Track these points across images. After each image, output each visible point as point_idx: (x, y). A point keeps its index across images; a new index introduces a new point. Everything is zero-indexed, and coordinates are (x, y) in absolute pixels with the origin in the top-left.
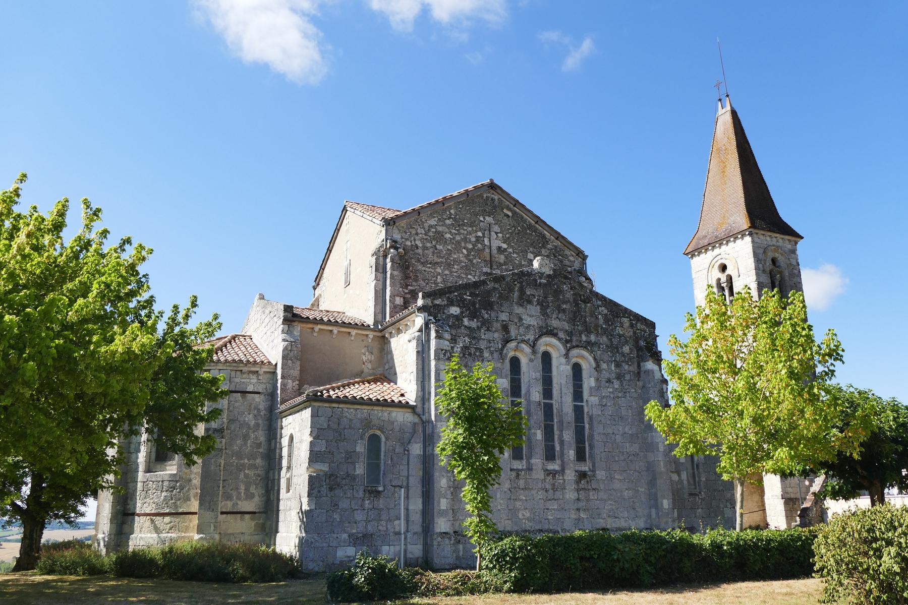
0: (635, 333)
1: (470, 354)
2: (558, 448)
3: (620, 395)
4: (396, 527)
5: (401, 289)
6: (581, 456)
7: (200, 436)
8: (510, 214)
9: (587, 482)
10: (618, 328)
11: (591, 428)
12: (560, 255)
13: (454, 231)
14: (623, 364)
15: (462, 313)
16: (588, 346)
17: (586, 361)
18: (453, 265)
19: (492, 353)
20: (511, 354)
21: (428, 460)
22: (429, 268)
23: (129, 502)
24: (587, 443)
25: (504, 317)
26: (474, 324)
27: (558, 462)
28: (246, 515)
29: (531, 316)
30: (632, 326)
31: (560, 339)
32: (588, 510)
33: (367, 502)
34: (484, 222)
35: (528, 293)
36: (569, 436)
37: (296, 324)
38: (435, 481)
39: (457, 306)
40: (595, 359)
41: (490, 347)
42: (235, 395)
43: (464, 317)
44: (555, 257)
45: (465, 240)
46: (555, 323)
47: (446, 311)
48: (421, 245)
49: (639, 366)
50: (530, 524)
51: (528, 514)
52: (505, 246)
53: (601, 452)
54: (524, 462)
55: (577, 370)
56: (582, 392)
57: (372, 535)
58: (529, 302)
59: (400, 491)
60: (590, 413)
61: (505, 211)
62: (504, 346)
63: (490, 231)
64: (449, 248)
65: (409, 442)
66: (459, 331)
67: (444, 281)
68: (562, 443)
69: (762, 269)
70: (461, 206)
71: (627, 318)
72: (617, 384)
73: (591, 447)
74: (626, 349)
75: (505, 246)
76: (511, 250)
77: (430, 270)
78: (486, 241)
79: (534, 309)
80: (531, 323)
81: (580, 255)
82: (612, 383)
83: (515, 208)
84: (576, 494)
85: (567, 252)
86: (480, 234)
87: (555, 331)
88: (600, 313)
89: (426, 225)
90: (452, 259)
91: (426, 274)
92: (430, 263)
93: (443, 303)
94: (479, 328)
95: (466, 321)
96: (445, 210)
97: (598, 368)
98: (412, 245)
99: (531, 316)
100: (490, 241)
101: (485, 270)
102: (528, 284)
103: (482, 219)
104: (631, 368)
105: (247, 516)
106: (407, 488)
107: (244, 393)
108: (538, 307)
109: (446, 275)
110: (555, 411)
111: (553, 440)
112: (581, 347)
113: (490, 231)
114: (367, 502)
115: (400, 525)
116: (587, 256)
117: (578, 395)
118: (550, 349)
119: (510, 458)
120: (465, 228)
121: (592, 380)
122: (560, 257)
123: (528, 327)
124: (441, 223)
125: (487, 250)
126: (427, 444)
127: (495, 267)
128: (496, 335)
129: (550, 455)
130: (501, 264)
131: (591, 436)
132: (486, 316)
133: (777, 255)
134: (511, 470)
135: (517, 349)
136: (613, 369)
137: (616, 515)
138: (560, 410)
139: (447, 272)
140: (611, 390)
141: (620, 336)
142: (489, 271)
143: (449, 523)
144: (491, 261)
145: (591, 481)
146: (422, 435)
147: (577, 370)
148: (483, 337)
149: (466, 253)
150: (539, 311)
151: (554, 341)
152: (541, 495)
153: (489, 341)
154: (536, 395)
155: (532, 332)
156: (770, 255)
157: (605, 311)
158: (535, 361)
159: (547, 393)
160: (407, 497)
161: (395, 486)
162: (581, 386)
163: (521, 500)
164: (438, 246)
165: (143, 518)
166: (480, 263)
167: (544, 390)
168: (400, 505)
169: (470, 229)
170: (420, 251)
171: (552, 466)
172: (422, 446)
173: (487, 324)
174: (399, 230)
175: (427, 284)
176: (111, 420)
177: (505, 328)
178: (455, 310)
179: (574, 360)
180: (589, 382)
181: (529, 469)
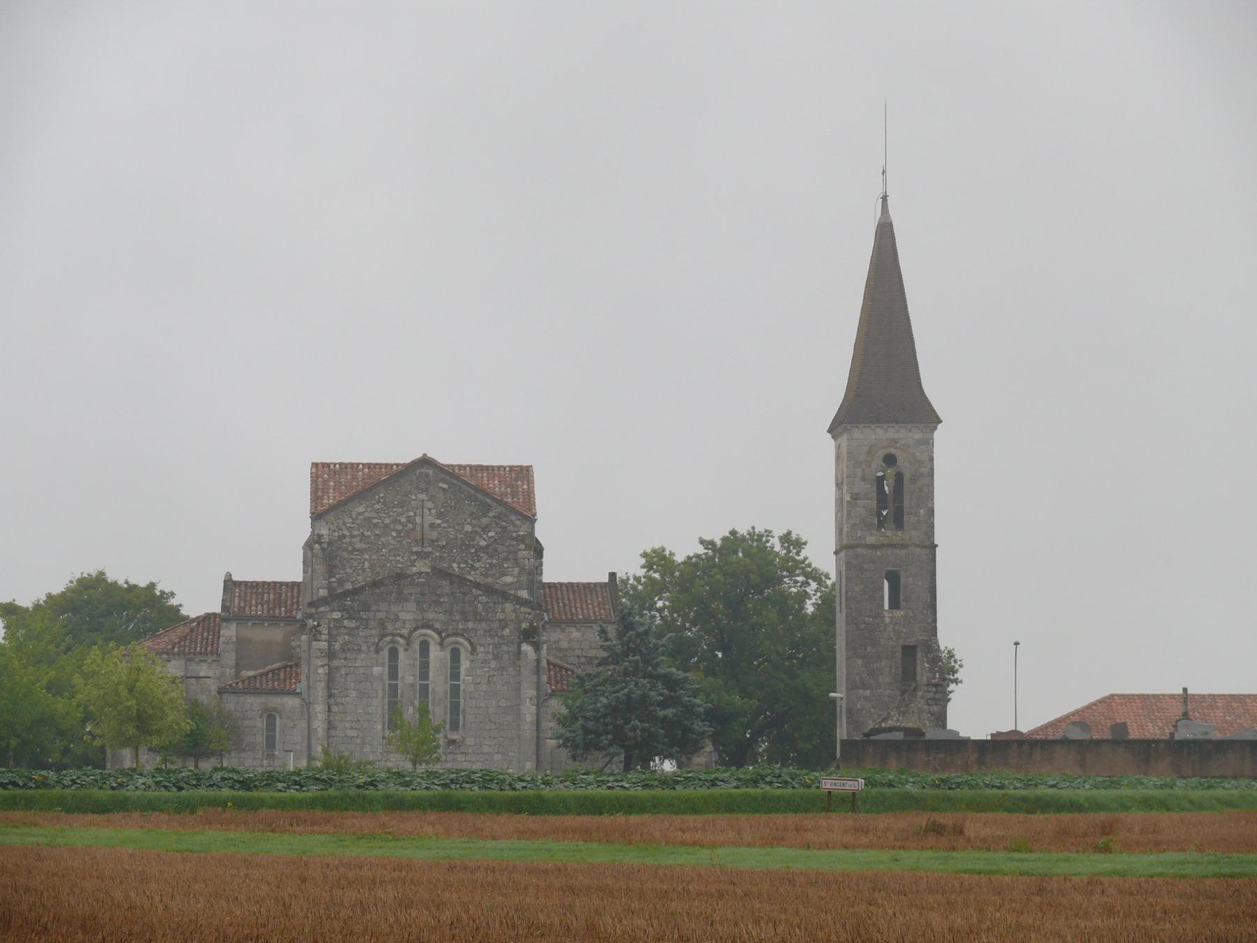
7: (817, 586)
8: (445, 486)
13: (383, 515)
18: (381, 549)
21: (310, 732)
25: (381, 615)
26: (353, 624)
31: (434, 630)
33: (265, 762)
34: (416, 500)
40: (471, 643)
42: (191, 679)
45: (396, 521)
46: (430, 615)
48: (348, 534)
52: (438, 522)
56: (428, 672)
58: (406, 600)
61: (440, 485)
67: (371, 567)
72: (493, 664)
75: (438, 522)
76: (445, 525)
77: (358, 557)
78: (418, 520)
79: (412, 606)
85: (513, 517)
87: (431, 623)
90: (380, 543)
92: (357, 551)
95: (346, 622)
98: (339, 536)
99: (408, 614)
101: (415, 549)
103: (413, 497)
107: (198, 678)
108: (415, 604)
110: (430, 690)
113: (423, 508)
122: (504, 523)
123: (404, 622)
125: (418, 529)
127: (426, 544)
128: (373, 632)
130: (433, 541)
135: (392, 641)
141: (500, 621)
148: (361, 634)
151: (429, 632)
153: (366, 637)
156: (881, 453)
159: (424, 675)
164: (366, 533)
169: (401, 510)
170: (347, 540)
173: (365, 623)
176: (64, 787)
177: (382, 624)
178: (337, 615)
180: (465, 664)
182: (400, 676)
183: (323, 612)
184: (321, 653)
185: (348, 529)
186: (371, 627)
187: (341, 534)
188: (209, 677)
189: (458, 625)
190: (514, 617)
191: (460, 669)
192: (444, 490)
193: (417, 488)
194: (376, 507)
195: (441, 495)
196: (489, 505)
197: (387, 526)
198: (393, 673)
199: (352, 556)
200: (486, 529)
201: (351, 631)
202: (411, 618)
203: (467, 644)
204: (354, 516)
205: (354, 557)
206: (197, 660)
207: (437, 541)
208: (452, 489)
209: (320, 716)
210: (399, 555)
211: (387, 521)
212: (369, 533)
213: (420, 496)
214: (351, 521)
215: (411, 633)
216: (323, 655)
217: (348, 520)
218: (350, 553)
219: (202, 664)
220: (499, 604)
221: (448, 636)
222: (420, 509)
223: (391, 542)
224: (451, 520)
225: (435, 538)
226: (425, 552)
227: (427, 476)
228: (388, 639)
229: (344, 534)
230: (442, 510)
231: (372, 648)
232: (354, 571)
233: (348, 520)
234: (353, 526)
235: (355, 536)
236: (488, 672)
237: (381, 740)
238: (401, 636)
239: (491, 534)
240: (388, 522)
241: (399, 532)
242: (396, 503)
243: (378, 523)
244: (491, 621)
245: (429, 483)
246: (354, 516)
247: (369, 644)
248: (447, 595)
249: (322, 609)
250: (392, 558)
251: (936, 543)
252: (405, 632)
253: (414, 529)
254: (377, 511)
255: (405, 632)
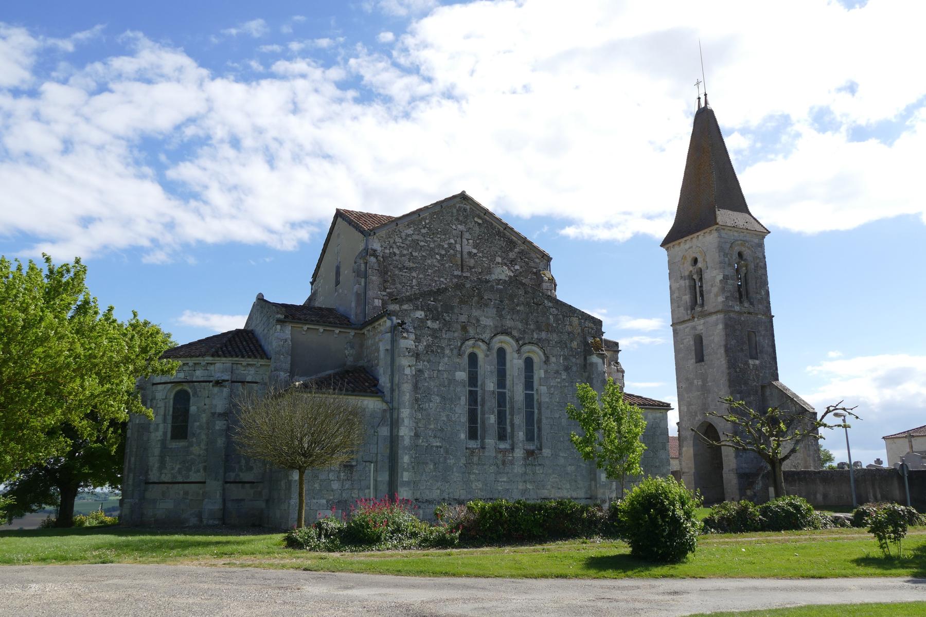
0: (583, 330)
1: (432, 351)
2: (509, 430)
3: (567, 384)
4: (367, 495)
5: (379, 292)
6: (530, 437)
8: (480, 221)
9: (534, 458)
10: (567, 326)
11: (540, 413)
12: (526, 258)
13: (429, 239)
14: (571, 358)
15: (426, 316)
16: (538, 343)
17: (537, 355)
18: (427, 270)
19: (452, 350)
20: (469, 351)
21: (394, 440)
22: (406, 272)
23: (150, 472)
24: (535, 426)
25: (463, 318)
26: (436, 325)
27: (509, 441)
28: (246, 485)
29: (488, 319)
30: (580, 324)
31: (513, 337)
32: (534, 482)
33: (342, 474)
35: (486, 297)
36: (519, 420)
37: (287, 324)
38: (399, 457)
39: (422, 310)
40: (545, 354)
41: (450, 345)
42: (236, 384)
43: (427, 320)
44: (522, 259)
46: (509, 323)
47: (412, 315)
49: (585, 359)
50: (482, 494)
51: (480, 486)
52: (475, 251)
53: (548, 434)
54: (479, 442)
55: (529, 363)
57: (346, 501)
58: (486, 305)
59: (370, 465)
60: (539, 400)
61: (476, 219)
62: (462, 344)
63: (461, 238)
64: (424, 254)
65: (379, 425)
66: (423, 331)
67: (419, 284)
68: (512, 425)
69: (727, 262)
70: (435, 216)
71: (576, 317)
73: (540, 429)
74: (575, 344)
75: (475, 251)
76: (481, 255)
78: (458, 247)
79: (492, 311)
80: (487, 324)
81: (545, 257)
82: (561, 374)
83: (485, 217)
84: (524, 469)
86: (452, 241)
87: (509, 330)
88: (551, 314)
89: (403, 235)
91: (403, 277)
92: (407, 269)
93: (410, 308)
94: (440, 330)
95: (429, 323)
96: (421, 221)
97: (547, 361)
99: (488, 319)
100: (461, 246)
101: (456, 273)
102: (485, 291)
104: (578, 361)
105: (248, 486)
106: (376, 462)
107: (243, 382)
109: (421, 278)
110: (508, 398)
111: (505, 424)
112: (533, 343)
113: (461, 238)
114: (342, 474)
115: (370, 493)
116: (551, 259)
117: (529, 385)
118: (504, 345)
119: (466, 438)
120: (439, 236)
121: (542, 372)
122: (527, 260)
124: (416, 233)
125: (459, 255)
126: (394, 427)
129: (502, 436)
130: (471, 268)
131: (540, 421)
132: (447, 318)
133: (743, 249)
134: (466, 448)
135: (474, 346)
136: (562, 362)
137: (559, 487)
138: (512, 398)
139: (421, 276)
140: (559, 380)
142: (459, 273)
143: (411, 492)
144: (462, 265)
145: (537, 458)
146: (389, 420)
147: (529, 363)
148: (444, 336)
149: (439, 258)
150: (495, 313)
151: (508, 339)
152: (493, 469)
153: (449, 340)
154: (491, 385)
155: (488, 331)
156: (737, 249)
157: (556, 312)
158: (490, 357)
159: (501, 383)
160: (376, 471)
161: (366, 462)
162: (532, 377)
163: (474, 473)
164: (414, 254)
165: (907, 444)
166: (452, 267)
167: (498, 380)
168: (370, 476)
169: (444, 237)
170: (397, 257)
171: (502, 446)
172: (389, 429)
173: (447, 325)
174: (379, 240)
175: (403, 286)
177: (464, 328)
179: (526, 355)
180: (539, 373)
181: (483, 448)
182: (479, 383)
183: (406, 310)
184: (409, 353)
185: (398, 247)
186: (454, 330)
187: (391, 251)
188: (256, 383)
189: (533, 334)
190: (580, 330)
191: (533, 379)
192: (479, 224)
193: (457, 219)
194: (423, 231)
195: (477, 228)
196: (514, 242)
197: (432, 249)
198: (473, 379)
199: (401, 273)
200: (513, 262)
201: (434, 334)
202: (491, 324)
203: (541, 353)
204: (404, 237)
205: (404, 274)
206: (244, 363)
207: (474, 267)
208: (486, 225)
209: (406, 422)
210: (443, 277)
211: (432, 245)
212: (417, 254)
213: (459, 227)
214: (401, 241)
215: (492, 338)
216: (411, 354)
217: (398, 240)
218: (400, 269)
219: (250, 368)
220: (567, 317)
221: (525, 344)
222: (459, 238)
223: (435, 264)
224: (485, 251)
225: (472, 265)
226: (464, 277)
227: (465, 210)
228: (471, 342)
229: (394, 252)
230: (478, 242)
231: (455, 352)
232: (403, 286)
233: (398, 240)
234: (402, 245)
235: (404, 255)
236: (560, 383)
237: (465, 451)
238: (483, 341)
239: (517, 267)
240: (433, 246)
241: (442, 256)
242: (439, 230)
243: (425, 245)
244: (561, 333)
245: (466, 217)
246: (404, 237)
247: (452, 347)
248: (523, 303)
249: (405, 307)
250: (436, 279)
251: (772, 314)
252: (486, 336)
253: (455, 255)
254: (424, 235)
255: (486, 336)
